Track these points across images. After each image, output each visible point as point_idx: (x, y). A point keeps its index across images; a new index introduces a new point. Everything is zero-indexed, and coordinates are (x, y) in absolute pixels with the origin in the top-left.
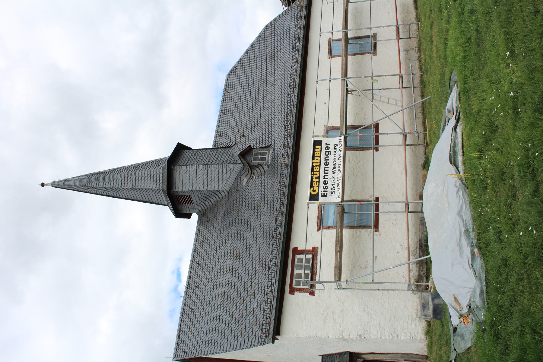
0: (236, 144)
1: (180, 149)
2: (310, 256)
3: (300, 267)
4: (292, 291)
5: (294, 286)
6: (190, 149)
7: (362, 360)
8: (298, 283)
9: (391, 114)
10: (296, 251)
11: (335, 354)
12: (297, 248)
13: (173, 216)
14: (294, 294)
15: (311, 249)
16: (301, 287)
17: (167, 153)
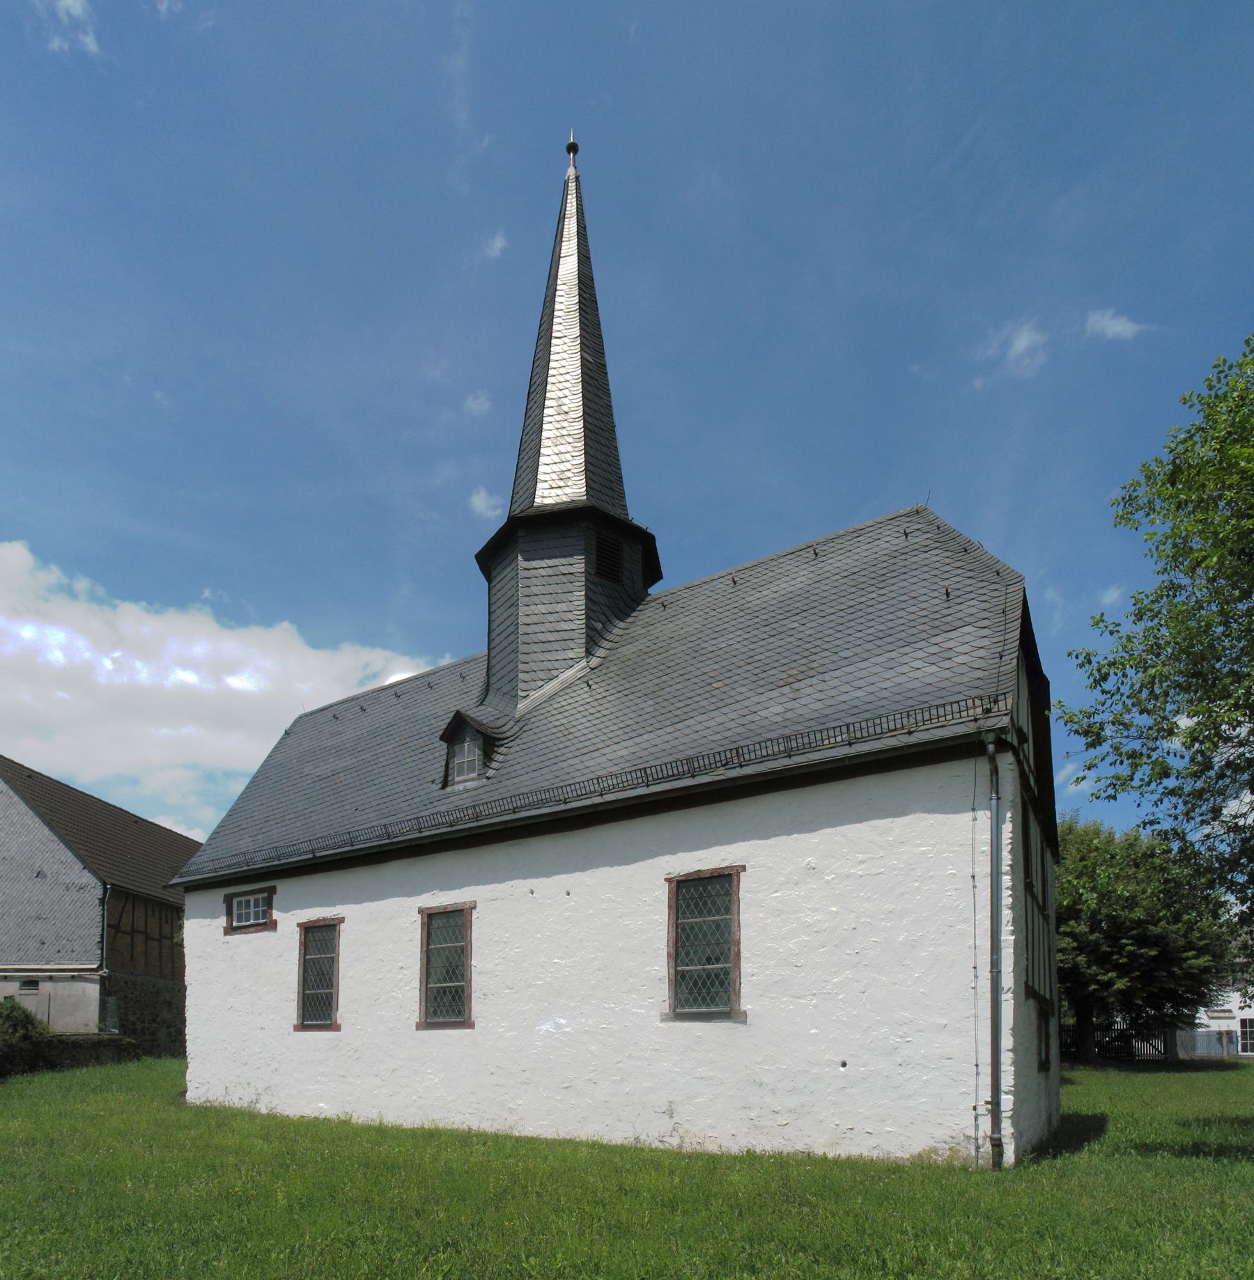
10: (272, 891)
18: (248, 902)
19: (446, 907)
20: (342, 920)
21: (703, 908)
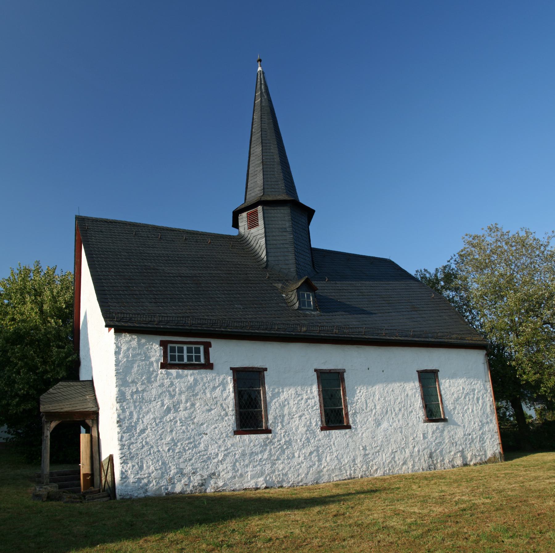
0: (318, 273)
1: (309, 213)
2: (202, 361)
3: (189, 350)
4: (163, 344)
5: (169, 346)
6: (309, 224)
7: (91, 426)
8: (173, 350)
9: (251, 128)
10: (207, 346)
11: (95, 395)
12: (211, 347)
13: (234, 209)
14: (212, 364)
15: (211, 362)
16: (169, 354)
17: (303, 200)
18: (181, 350)
19: (330, 370)
20: (266, 369)
21: (428, 379)
